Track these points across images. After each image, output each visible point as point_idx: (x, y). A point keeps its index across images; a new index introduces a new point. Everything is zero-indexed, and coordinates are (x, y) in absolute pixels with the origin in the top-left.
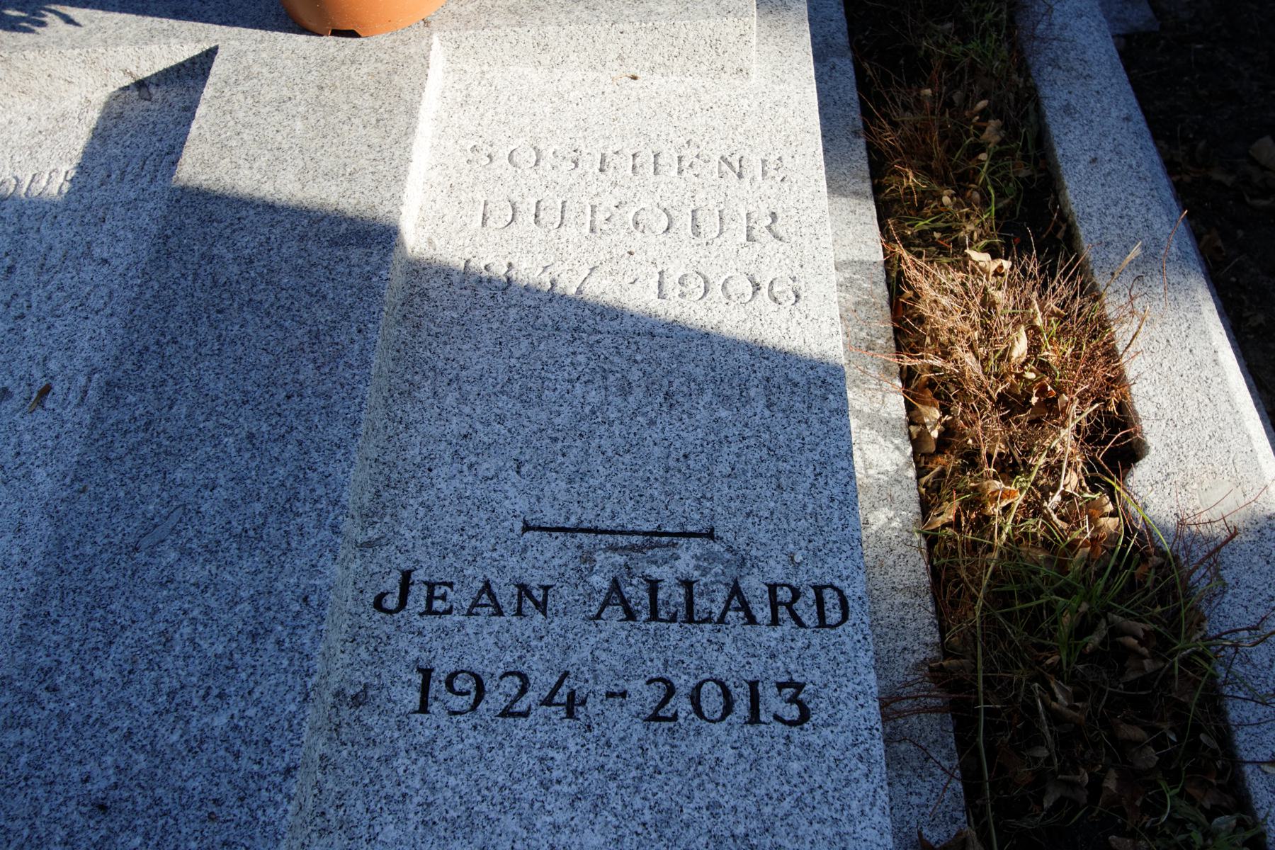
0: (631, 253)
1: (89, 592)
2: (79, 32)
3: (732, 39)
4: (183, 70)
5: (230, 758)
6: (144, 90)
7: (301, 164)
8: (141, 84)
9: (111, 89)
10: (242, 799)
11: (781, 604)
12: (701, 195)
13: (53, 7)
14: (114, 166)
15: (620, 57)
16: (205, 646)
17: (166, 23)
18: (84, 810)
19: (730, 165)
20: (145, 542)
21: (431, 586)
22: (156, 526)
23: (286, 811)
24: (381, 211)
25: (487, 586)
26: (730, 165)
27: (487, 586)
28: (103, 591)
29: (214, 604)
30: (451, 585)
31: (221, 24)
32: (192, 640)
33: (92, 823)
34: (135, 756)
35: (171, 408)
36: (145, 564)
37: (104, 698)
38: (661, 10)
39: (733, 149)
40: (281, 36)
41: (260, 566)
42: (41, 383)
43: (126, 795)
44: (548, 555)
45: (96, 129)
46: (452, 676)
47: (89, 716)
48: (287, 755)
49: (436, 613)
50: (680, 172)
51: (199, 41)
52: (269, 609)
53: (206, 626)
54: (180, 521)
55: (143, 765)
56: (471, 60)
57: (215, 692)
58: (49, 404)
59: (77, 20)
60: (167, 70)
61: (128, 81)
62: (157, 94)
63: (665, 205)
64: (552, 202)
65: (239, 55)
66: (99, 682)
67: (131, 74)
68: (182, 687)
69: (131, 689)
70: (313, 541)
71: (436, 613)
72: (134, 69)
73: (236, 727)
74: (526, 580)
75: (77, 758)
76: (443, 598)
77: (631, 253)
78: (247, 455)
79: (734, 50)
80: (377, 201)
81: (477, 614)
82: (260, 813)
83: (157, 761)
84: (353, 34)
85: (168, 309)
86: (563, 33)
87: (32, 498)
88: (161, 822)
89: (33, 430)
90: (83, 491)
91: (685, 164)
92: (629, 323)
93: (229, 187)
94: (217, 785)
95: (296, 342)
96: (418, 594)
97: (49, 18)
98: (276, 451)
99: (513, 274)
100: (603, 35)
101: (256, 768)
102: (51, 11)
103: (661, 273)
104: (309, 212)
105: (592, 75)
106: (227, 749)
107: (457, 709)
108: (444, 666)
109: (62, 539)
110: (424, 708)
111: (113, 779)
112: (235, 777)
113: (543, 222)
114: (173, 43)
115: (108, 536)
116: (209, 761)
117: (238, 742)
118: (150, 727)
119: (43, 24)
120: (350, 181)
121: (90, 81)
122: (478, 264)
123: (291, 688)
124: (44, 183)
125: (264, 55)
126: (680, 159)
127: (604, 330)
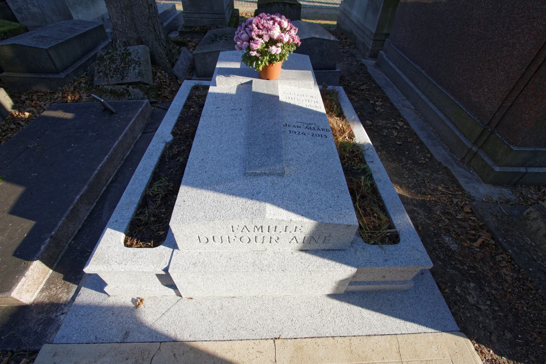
8: (241, 84)
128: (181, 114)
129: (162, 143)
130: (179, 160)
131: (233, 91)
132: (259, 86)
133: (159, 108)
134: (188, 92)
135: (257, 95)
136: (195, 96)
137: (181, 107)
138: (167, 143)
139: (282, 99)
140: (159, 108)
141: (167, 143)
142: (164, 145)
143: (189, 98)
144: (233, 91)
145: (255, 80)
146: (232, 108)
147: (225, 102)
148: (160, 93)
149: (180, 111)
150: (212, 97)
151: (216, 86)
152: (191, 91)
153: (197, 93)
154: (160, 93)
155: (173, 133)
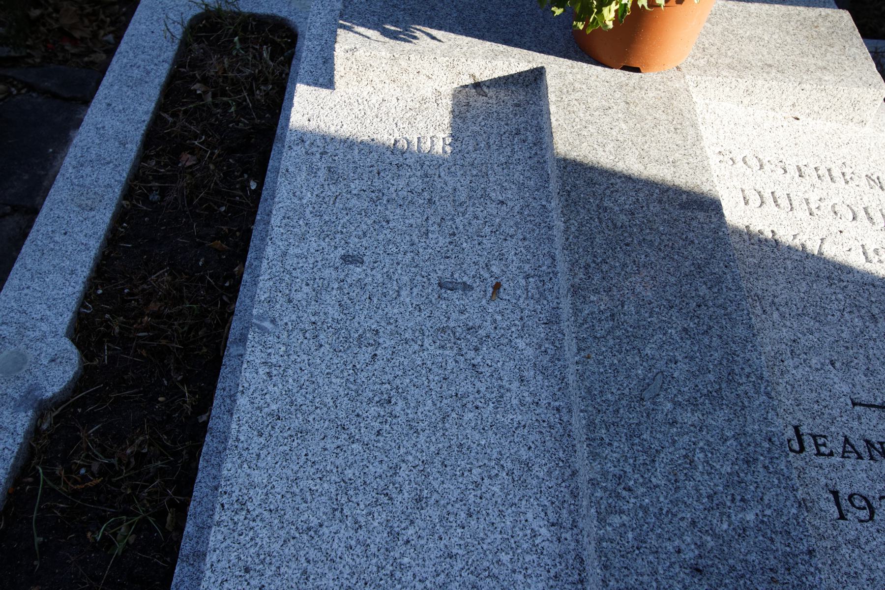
0: (841, 232)
1: (623, 426)
2: (444, 46)
3: (867, 101)
4: (510, 80)
5: (768, 543)
6: (479, 89)
7: (638, 153)
8: (477, 85)
9: (455, 86)
10: (788, 569)
11: (821, 445)
12: (865, 199)
13: (418, 27)
14: (479, 138)
15: (794, 105)
16: (718, 467)
17: (502, 47)
18: (687, 571)
19: (873, 180)
20: (646, 395)
21: (814, 437)
22: (649, 385)
23: (820, 578)
24: (706, 188)
25: (847, 440)
26: (873, 180)
27: (847, 440)
28: (633, 426)
29: (712, 440)
30: (825, 437)
31: (540, 52)
32: (707, 462)
33: (696, 580)
34: (704, 537)
35: (623, 307)
36: (653, 410)
37: (666, 498)
38: (826, 78)
39: (872, 171)
40: (585, 65)
41: (731, 416)
42: (492, 281)
43: (710, 563)
44: (874, 422)
45: (453, 112)
46: (851, 497)
47: (661, 509)
48: (804, 541)
49: (823, 454)
50: (847, 182)
51: (529, 62)
52: (749, 445)
53: (712, 453)
54: (663, 383)
55: (712, 543)
56: (700, 95)
57: (739, 498)
58: (502, 294)
59: (438, 37)
60: (499, 78)
61: (470, 81)
62: (491, 93)
63: (848, 203)
64: (781, 194)
65: (561, 75)
66: (656, 486)
67: (474, 77)
68: (715, 493)
69: (681, 492)
70: (758, 403)
71: (823, 454)
72: (477, 75)
73: (762, 522)
74: (868, 437)
75: (666, 536)
76: (824, 445)
77: (841, 232)
78: (689, 342)
79: (865, 109)
80: (699, 183)
81: (848, 457)
82: (804, 579)
83: (721, 541)
84: (637, 70)
85: (592, 239)
86: (766, 86)
87: (521, 359)
88: (742, 582)
89: (501, 313)
90: (589, 357)
91: (848, 177)
92: (858, 277)
93: (595, 162)
94: (767, 559)
95: (687, 270)
96: (808, 441)
97: (418, 34)
98: (706, 341)
99: (777, 237)
100: (791, 89)
101: (788, 549)
102: (417, 30)
103: (863, 246)
104: (657, 184)
105: (771, 114)
106: (763, 536)
107: (863, 518)
108: (844, 490)
109: (589, 390)
110: (842, 517)
111: (697, 552)
112: (777, 554)
113: (782, 206)
114: (515, 61)
115: (619, 389)
116: (755, 543)
117: (769, 532)
118: (705, 518)
119: (415, 38)
120: (674, 167)
121: (444, 79)
122: (755, 228)
123: (787, 498)
124: (429, 144)
125: (579, 76)
126: (843, 174)
127: (845, 279)
128: (128, 193)
129: (18, 406)
130: (108, 542)
131: (432, 133)
132: (593, 115)
133: (31, 88)
134: (170, 53)
135: (586, 183)
136: (205, 80)
137: (133, 149)
138: (42, 408)
139: (736, 215)
140: (31, 88)
141: (42, 408)
142: (23, 420)
143: (174, 91)
144: (432, 133)
145: (563, 75)
146: (443, 270)
147: (394, 213)
148: (35, 13)
149: (126, 168)
150: (313, 171)
151: (329, 83)
152: (185, 46)
153: (215, 66)
154: (35, 13)
155: (83, 331)
